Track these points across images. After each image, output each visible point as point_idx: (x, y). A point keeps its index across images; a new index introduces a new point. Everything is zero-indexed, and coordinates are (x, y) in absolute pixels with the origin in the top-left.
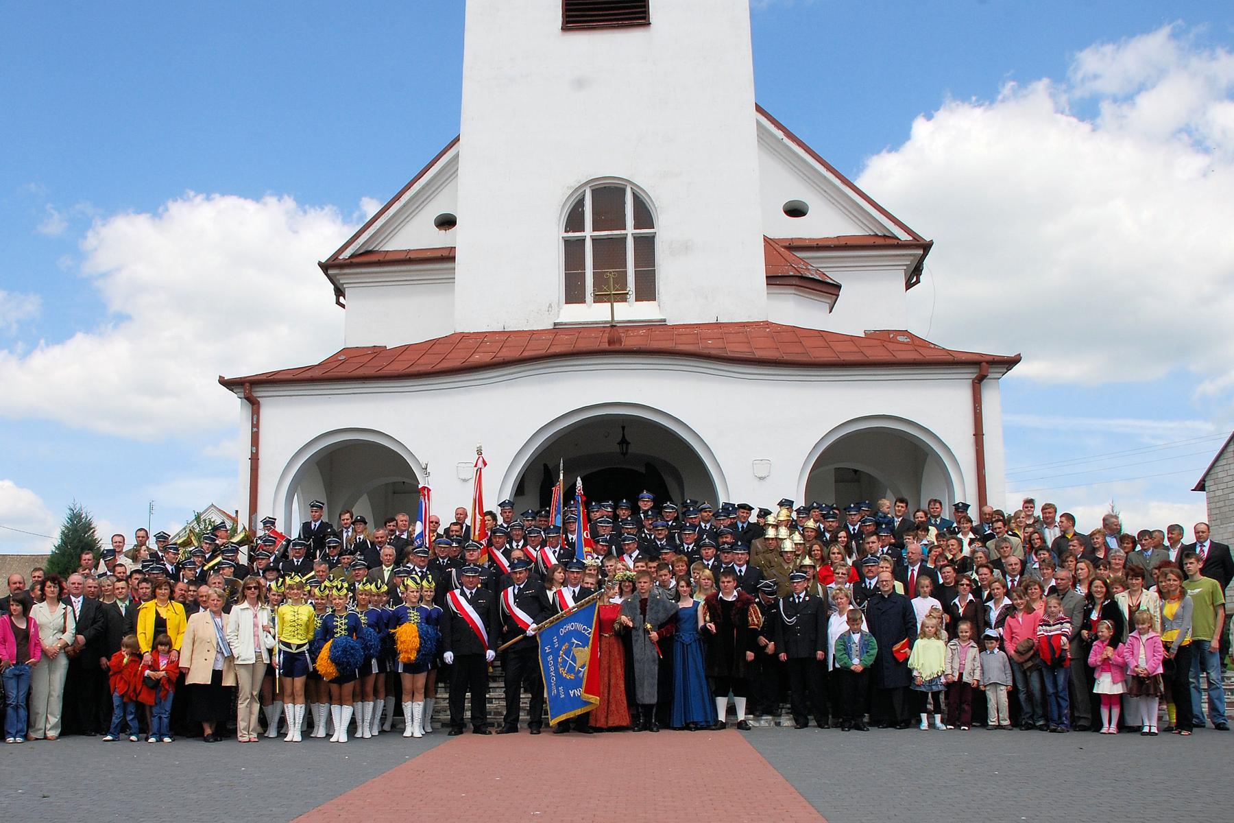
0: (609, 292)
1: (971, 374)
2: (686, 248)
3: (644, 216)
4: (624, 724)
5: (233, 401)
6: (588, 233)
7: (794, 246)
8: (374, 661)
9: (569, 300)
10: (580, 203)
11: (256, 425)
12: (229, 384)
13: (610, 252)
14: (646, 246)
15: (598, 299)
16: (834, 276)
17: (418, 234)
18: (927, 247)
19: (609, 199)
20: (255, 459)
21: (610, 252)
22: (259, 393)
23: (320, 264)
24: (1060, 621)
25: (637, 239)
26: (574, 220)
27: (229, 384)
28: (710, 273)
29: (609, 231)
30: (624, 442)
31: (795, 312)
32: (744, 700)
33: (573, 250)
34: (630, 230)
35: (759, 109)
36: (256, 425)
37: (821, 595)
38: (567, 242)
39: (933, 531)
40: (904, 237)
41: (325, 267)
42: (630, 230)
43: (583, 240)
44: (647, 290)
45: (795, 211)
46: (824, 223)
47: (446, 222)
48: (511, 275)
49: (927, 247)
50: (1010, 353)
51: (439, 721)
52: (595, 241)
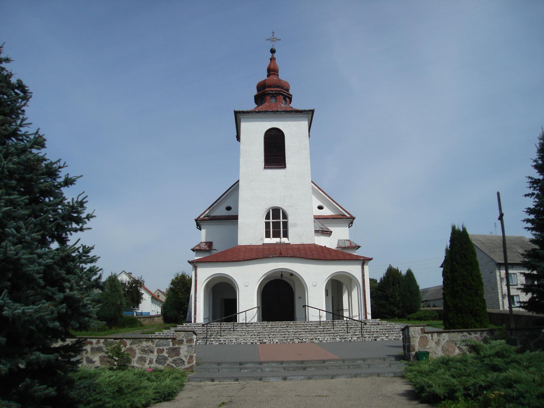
0: (276, 235)
2: (295, 225)
3: (285, 216)
4: (412, 328)
5: (191, 266)
6: (271, 220)
11: (196, 272)
13: (276, 225)
14: (285, 225)
15: (274, 236)
16: (331, 229)
17: (221, 211)
18: (354, 219)
19: (276, 212)
22: (198, 265)
24: (399, 308)
25: (283, 222)
26: (268, 217)
28: (301, 233)
29: (277, 221)
30: (282, 275)
31: (322, 241)
33: (267, 225)
34: (281, 220)
35: (312, 182)
36: (196, 272)
38: (266, 222)
40: (348, 216)
42: (281, 220)
43: (269, 222)
44: (286, 235)
45: (320, 208)
46: (327, 212)
47: (229, 209)
48: (251, 231)
52: (280, 219)
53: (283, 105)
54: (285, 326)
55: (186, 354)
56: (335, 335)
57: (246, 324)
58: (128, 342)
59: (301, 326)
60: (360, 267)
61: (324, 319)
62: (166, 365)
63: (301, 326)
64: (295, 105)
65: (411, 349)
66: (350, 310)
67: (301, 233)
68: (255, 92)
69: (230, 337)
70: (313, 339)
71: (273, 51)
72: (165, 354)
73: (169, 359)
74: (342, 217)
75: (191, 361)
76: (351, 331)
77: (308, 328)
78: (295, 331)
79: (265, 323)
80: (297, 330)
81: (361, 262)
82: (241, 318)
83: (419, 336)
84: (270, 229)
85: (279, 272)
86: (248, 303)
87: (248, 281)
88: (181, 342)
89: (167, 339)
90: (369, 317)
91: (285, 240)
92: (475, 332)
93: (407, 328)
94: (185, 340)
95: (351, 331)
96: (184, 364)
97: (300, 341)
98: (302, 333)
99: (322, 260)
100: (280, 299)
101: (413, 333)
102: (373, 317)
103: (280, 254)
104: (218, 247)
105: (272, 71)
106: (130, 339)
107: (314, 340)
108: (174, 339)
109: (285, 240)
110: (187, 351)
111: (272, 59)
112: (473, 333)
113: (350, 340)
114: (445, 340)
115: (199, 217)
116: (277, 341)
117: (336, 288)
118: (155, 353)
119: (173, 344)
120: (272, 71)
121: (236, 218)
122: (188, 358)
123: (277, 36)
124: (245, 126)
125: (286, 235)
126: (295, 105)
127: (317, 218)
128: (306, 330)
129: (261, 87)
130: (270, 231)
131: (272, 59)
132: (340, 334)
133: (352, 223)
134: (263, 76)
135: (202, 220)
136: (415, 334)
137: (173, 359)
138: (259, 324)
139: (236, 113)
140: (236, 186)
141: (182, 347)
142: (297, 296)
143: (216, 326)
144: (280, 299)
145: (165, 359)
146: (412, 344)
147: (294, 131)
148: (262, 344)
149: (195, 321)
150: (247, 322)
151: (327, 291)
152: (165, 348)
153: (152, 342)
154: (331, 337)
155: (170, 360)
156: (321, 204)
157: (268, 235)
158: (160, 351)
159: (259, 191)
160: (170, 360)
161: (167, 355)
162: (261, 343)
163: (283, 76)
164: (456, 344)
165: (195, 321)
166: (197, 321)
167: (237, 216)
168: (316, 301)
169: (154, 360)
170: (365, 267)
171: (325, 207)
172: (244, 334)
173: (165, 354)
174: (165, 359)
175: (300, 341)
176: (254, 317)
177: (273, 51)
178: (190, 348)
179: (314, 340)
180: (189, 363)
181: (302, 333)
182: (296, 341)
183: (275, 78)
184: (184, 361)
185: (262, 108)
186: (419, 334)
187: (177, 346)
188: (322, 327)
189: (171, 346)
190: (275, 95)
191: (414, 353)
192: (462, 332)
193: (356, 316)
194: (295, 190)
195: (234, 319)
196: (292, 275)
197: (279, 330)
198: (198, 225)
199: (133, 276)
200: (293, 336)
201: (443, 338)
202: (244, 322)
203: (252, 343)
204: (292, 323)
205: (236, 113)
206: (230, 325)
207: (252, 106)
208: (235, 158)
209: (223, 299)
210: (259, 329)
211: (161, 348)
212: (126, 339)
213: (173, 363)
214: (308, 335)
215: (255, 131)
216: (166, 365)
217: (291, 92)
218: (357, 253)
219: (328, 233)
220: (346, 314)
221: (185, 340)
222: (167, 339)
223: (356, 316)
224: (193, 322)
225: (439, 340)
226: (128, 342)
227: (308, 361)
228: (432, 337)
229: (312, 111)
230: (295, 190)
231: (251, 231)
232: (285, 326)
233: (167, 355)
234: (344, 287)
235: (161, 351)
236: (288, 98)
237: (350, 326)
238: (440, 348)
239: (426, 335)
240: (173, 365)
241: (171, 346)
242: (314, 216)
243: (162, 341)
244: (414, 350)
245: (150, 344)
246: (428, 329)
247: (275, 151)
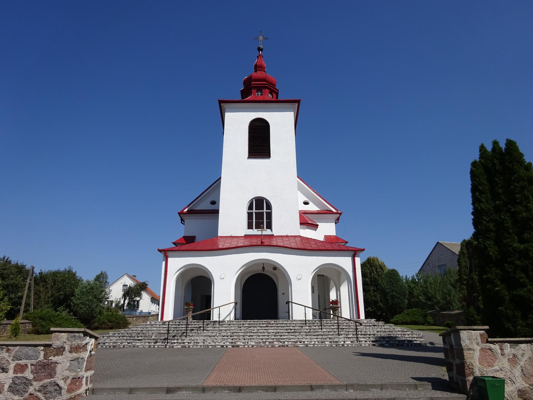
1: (352, 253)
3: (269, 207)
5: (161, 255)
6: (254, 210)
7: (305, 213)
9: (248, 229)
12: (160, 251)
13: (259, 216)
14: (269, 216)
16: (318, 223)
17: (205, 205)
18: (340, 214)
21: (259, 216)
22: (169, 253)
23: (178, 213)
26: (250, 207)
27: (160, 251)
28: (285, 223)
29: (260, 211)
30: (263, 268)
31: (308, 233)
32: (359, 258)
33: (250, 215)
34: (265, 210)
37: (52, 329)
38: (248, 213)
40: (334, 211)
41: (179, 214)
42: (265, 210)
44: (269, 226)
45: (306, 203)
46: (312, 207)
50: (363, 248)
54: (265, 325)
55: (67, 373)
56: (324, 337)
59: (283, 325)
60: (349, 259)
62: (27, 395)
63: (283, 325)
65: (467, 372)
69: (199, 339)
70: (297, 342)
72: (28, 374)
73: (34, 383)
74: (328, 212)
75: (73, 387)
76: (342, 333)
77: (291, 328)
78: (275, 331)
80: (278, 331)
82: (215, 317)
83: (479, 348)
84: (253, 220)
85: (258, 264)
86: (224, 299)
87: (225, 273)
91: (268, 232)
94: (67, 348)
95: (342, 333)
96: (60, 394)
97: (281, 344)
98: (284, 334)
99: (312, 213)
101: (468, 342)
102: (366, 317)
103: (262, 242)
107: (299, 343)
109: (268, 232)
110: (69, 369)
113: (343, 345)
114: (526, 358)
116: (253, 343)
117: (322, 281)
118: (11, 371)
119: (45, 356)
121: (217, 212)
122: (69, 381)
124: (229, 116)
128: (289, 331)
130: (252, 222)
132: (330, 336)
133: (338, 219)
134: (250, 72)
135: (185, 213)
136: (471, 343)
137: (41, 383)
138: (235, 323)
139: (221, 102)
140: (220, 178)
145: (27, 383)
146: (468, 361)
148: (235, 348)
150: (221, 319)
151: (313, 288)
152: (29, 362)
153: (8, 351)
154: (319, 340)
155: (36, 385)
156: (306, 199)
158: (21, 368)
160: (36, 385)
161: (31, 377)
162: (233, 346)
166: (165, 319)
169: (6, 387)
170: (356, 258)
171: (311, 203)
172: (214, 334)
173: (28, 374)
174: (27, 383)
175: (281, 344)
176: (229, 314)
178: (75, 363)
179: (299, 343)
180: (69, 391)
181: (284, 334)
184: (61, 388)
186: (478, 344)
188: (307, 328)
189: (41, 357)
190: (259, 89)
191: (471, 378)
195: (208, 316)
196: (275, 268)
197: (261, 330)
199: (137, 278)
200: (273, 337)
201: (521, 352)
202: (218, 320)
203: (222, 346)
204: (273, 322)
205: (221, 102)
207: (239, 98)
209: (197, 291)
210: (233, 328)
211: (22, 362)
213: (39, 391)
214: (291, 337)
216: (27, 395)
217: (277, 87)
219: (315, 226)
221: (67, 348)
225: (514, 355)
228: (501, 349)
229: (298, 102)
231: (232, 221)
232: (265, 325)
233: (31, 377)
234: (332, 283)
235: (21, 368)
237: (341, 327)
238: (517, 372)
239: (492, 346)
240: (40, 395)
242: (300, 211)
244: (473, 373)
247: (259, 142)
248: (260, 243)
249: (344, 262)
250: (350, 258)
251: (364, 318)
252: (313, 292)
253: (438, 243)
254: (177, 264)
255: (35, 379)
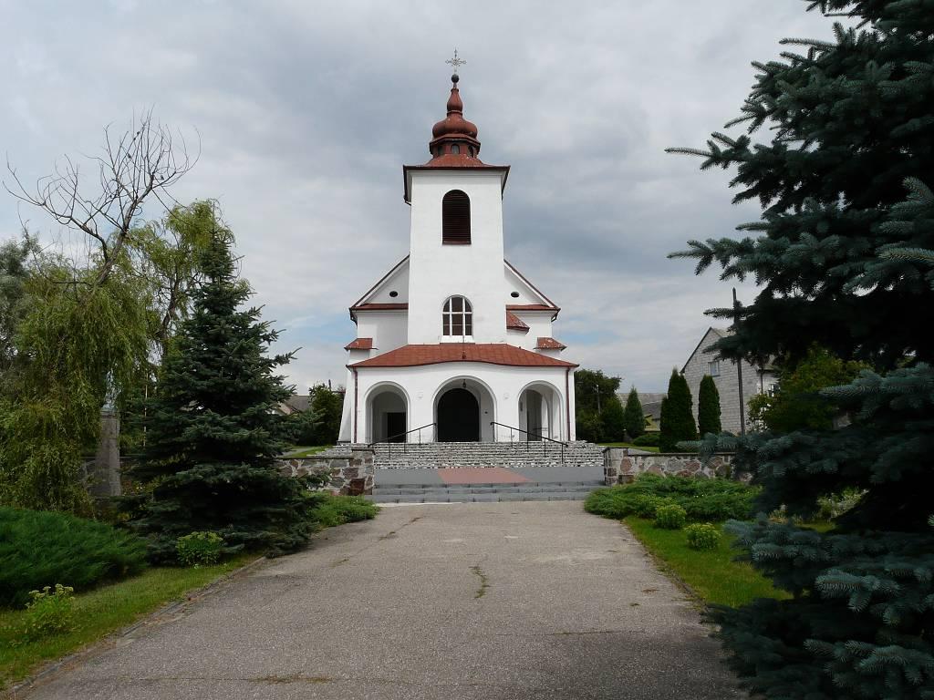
0: (457, 332)
3: (469, 308)
5: (350, 373)
6: (451, 313)
8: (698, 432)
10: (448, 302)
13: (457, 319)
14: (469, 318)
16: (528, 325)
17: (384, 299)
18: (559, 310)
19: (457, 302)
20: (356, 390)
21: (457, 319)
22: (358, 369)
25: (466, 315)
26: (446, 308)
28: (489, 329)
29: (458, 313)
30: (464, 384)
31: (516, 340)
33: (446, 318)
34: (464, 312)
35: (505, 261)
38: (444, 315)
39: (343, 477)
40: (551, 306)
42: (464, 312)
44: (469, 332)
45: (515, 295)
46: (523, 301)
47: (394, 294)
48: (425, 327)
49: (559, 310)
51: (33, 519)
52: (462, 311)
53: (466, 159)
57: (420, 444)
58: (300, 463)
60: (563, 377)
61: (516, 439)
64: (485, 157)
66: (550, 429)
67: (489, 329)
68: (431, 138)
71: (455, 79)
72: (341, 475)
79: (444, 444)
81: (566, 369)
82: (412, 438)
86: (421, 420)
87: (421, 393)
88: (359, 462)
89: (343, 459)
90: (573, 438)
91: (468, 339)
92: (685, 456)
93: (608, 449)
94: (364, 460)
100: (461, 413)
103: (464, 357)
104: (380, 348)
105: (454, 108)
106: (302, 459)
108: (351, 459)
111: (455, 91)
112: (682, 458)
115: (354, 306)
117: (533, 401)
120: (454, 108)
121: (404, 307)
123: (461, 57)
125: (469, 332)
126: (485, 157)
127: (510, 309)
129: (439, 131)
131: (455, 91)
133: (556, 315)
134: (441, 116)
139: (406, 169)
140: (406, 260)
141: (360, 467)
142: (483, 409)
143: (382, 447)
144: (461, 413)
147: (483, 197)
149: (355, 441)
152: (341, 469)
157: (446, 332)
159: (436, 273)
160: (348, 481)
161: (343, 477)
163: (468, 116)
164: (663, 469)
165: (355, 441)
167: (407, 304)
168: (506, 418)
173: (341, 475)
177: (455, 79)
182: (482, 465)
183: (459, 120)
185: (441, 161)
187: (354, 466)
189: (348, 466)
192: (670, 456)
193: (556, 437)
194: (481, 273)
195: (402, 439)
198: (352, 315)
205: (406, 169)
206: (400, 447)
207: (425, 157)
208: (403, 231)
209: (390, 418)
212: (297, 459)
215: (431, 194)
217: (479, 138)
218: (559, 357)
220: (545, 434)
222: (343, 459)
223: (556, 437)
224: (352, 442)
226: (300, 463)
227: (499, 484)
229: (506, 169)
230: (481, 273)
234: (543, 399)
236: (475, 147)
241: (348, 466)
243: (338, 461)
245: (324, 464)
246: (632, 451)
248: (461, 358)
249: (557, 380)
250: (736, 140)
251: (428, 435)
252: (521, 409)
253: (711, 329)
254: (370, 380)
255: (346, 478)
